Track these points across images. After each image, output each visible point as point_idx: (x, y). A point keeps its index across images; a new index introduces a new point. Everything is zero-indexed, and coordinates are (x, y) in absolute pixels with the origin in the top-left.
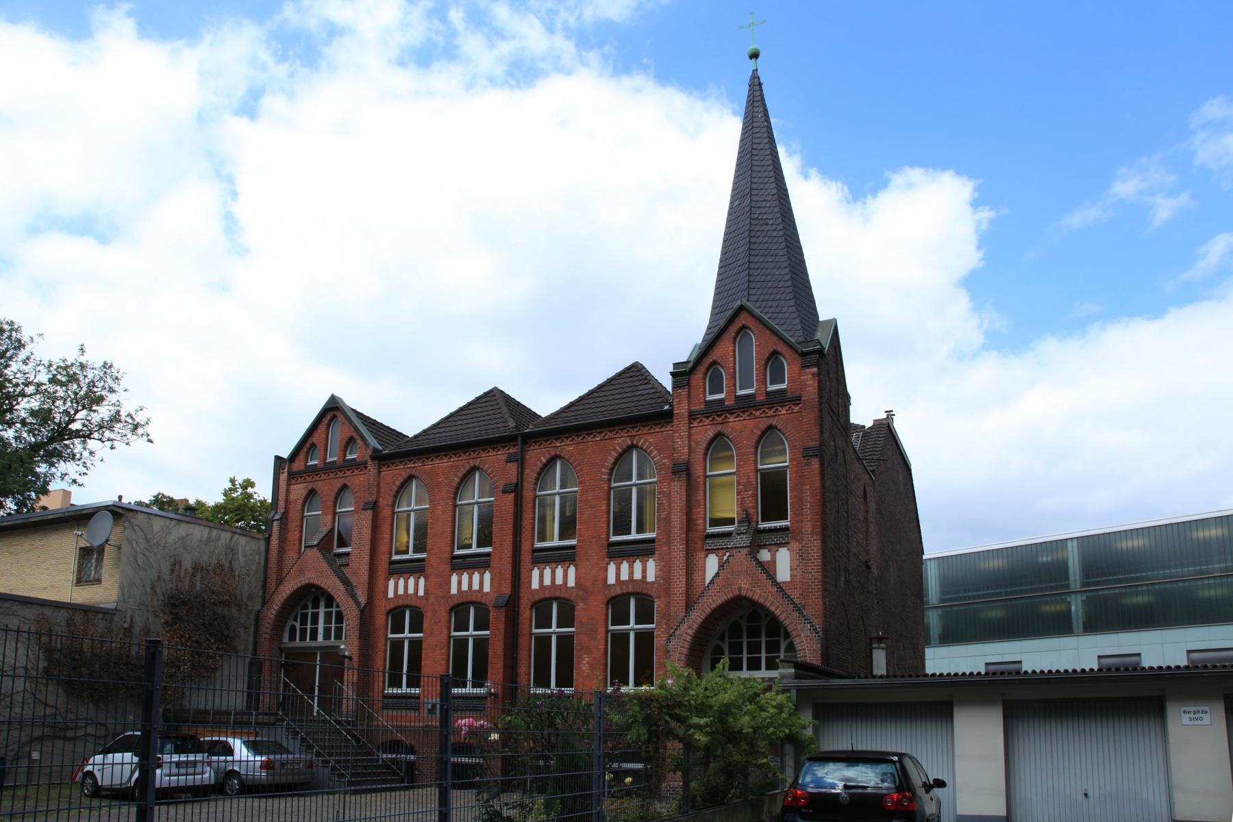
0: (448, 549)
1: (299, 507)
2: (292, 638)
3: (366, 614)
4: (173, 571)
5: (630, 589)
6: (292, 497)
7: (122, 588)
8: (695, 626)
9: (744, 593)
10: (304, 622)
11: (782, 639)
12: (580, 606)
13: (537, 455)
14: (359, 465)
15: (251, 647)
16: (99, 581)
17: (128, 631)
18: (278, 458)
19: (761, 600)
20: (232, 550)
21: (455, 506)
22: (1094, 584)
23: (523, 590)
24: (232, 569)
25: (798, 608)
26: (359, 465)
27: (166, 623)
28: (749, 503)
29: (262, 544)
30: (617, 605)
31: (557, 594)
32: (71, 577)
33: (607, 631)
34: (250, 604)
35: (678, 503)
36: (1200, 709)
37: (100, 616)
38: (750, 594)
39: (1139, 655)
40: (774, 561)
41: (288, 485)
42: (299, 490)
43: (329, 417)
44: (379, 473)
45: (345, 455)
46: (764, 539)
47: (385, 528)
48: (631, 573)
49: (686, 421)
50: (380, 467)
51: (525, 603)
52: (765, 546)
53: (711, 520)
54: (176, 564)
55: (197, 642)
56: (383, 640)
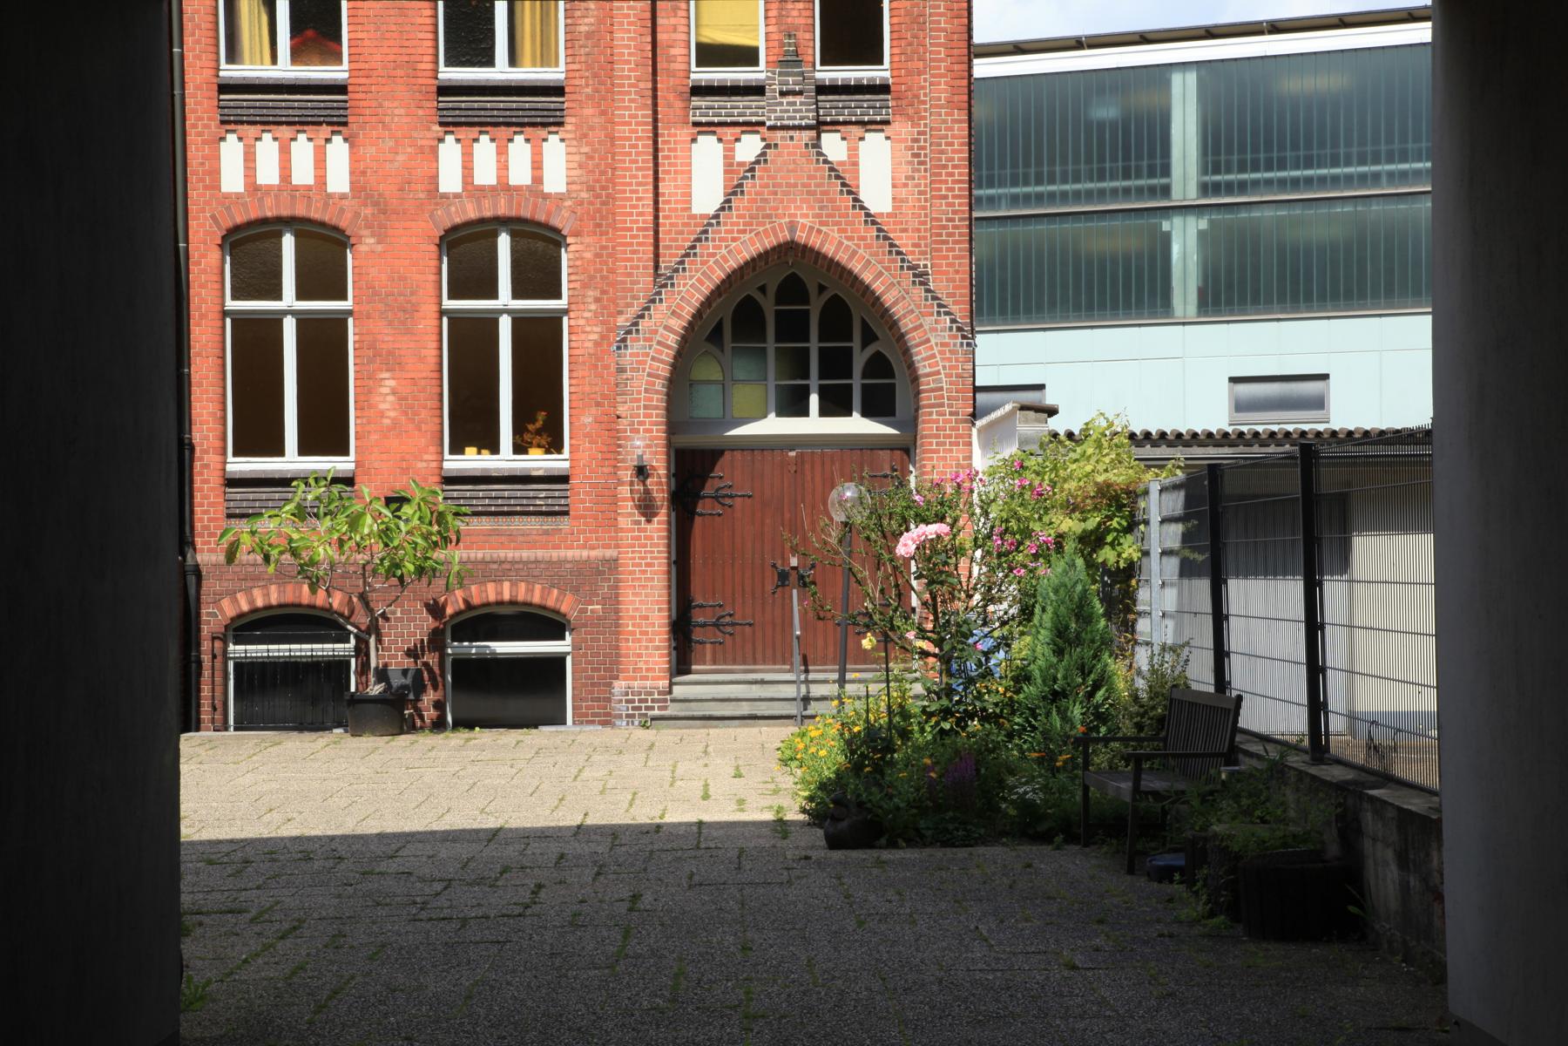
5: (503, 210)
8: (688, 311)
9: (801, 237)
11: (856, 344)
12: (367, 243)
22: (1229, 188)
25: (921, 277)
30: (465, 252)
31: (300, 211)
38: (815, 241)
39: (1325, 377)
48: (503, 167)
53: (699, 46)
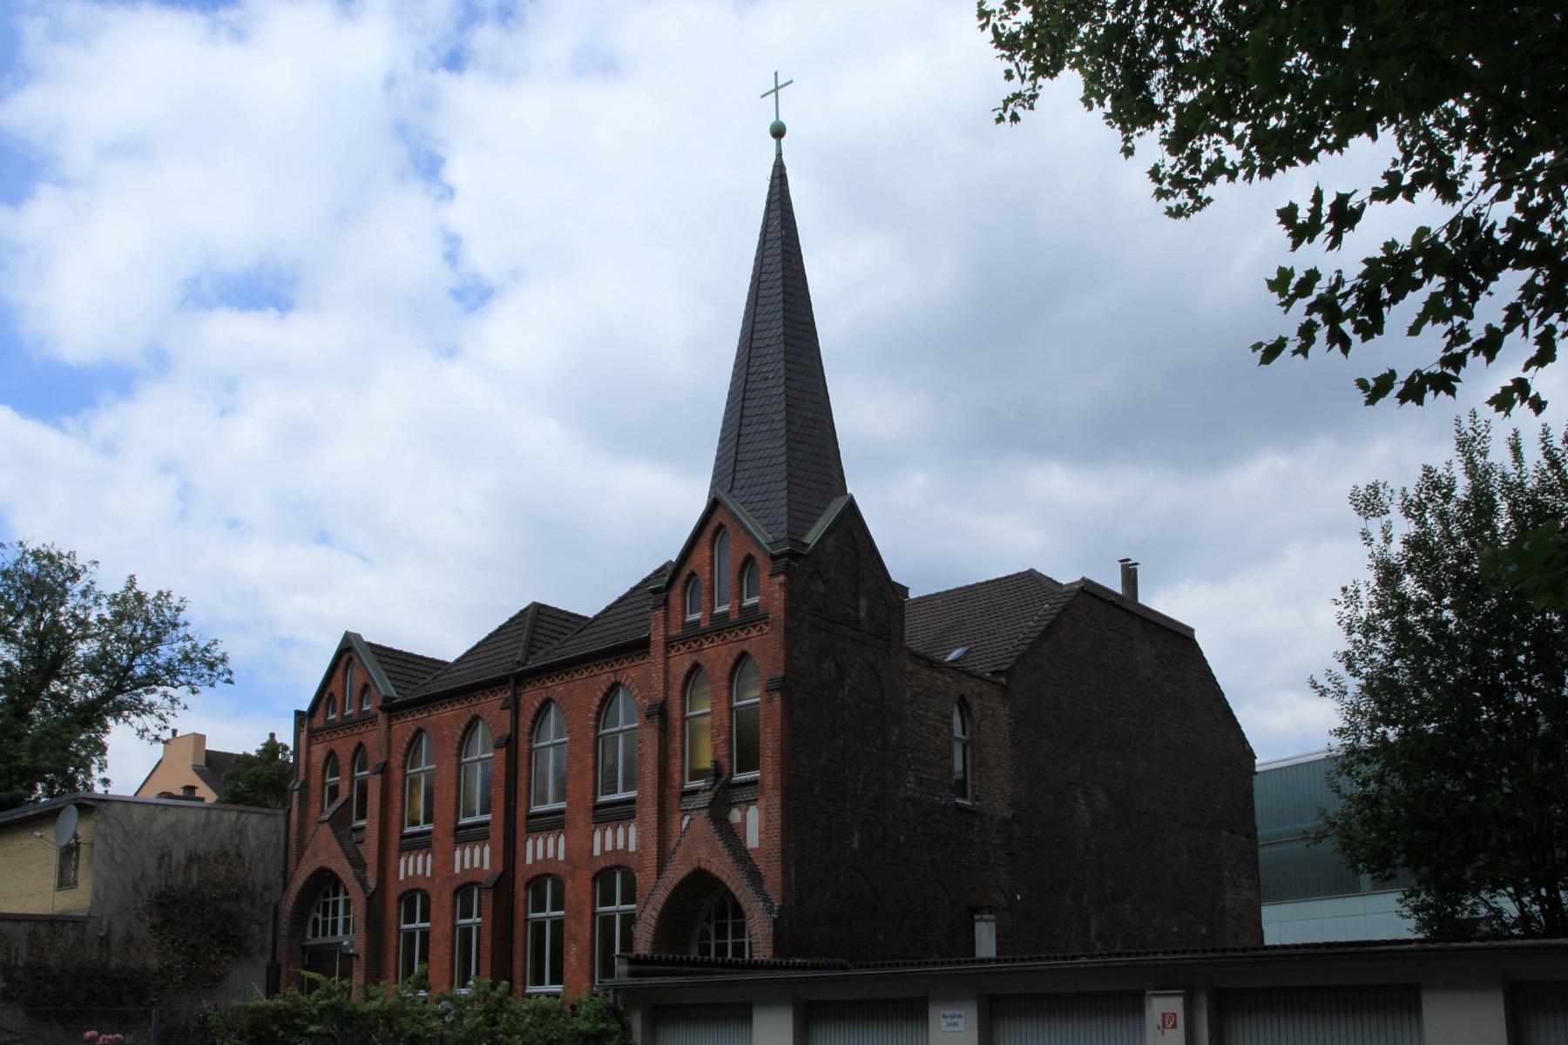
0: (452, 818)
1: (319, 773)
2: (315, 934)
3: (375, 903)
4: (160, 865)
6: (313, 760)
7: (95, 891)
9: (703, 865)
10: (325, 915)
13: (531, 698)
14: (367, 719)
15: (269, 947)
16: (76, 883)
17: (105, 941)
18: (298, 714)
19: (718, 874)
20: (239, 832)
21: (459, 765)
23: (518, 866)
24: (240, 856)
26: (367, 719)
27: (154, 927)
28: (723, 751)
29: (281, 821)
32: (52, 880)
33: (594, 914)
34: (266, 896)
35: (650, 751)
36: (957, 1012)
37: (70, 925)
38: (708, 867)
40: (744, 823)
41: (309, 746)
42: (319, 752)
43: (345, 659)
44: (389, 727)
45: (361, 706)
46: (738, 796)
47: (396, 795)
49: (661, 651)
50: (390, 721)
51: (520, 882)
52: (734, 805)
54: (164, 856)
55: (193, 946)
56: (393, 934)
